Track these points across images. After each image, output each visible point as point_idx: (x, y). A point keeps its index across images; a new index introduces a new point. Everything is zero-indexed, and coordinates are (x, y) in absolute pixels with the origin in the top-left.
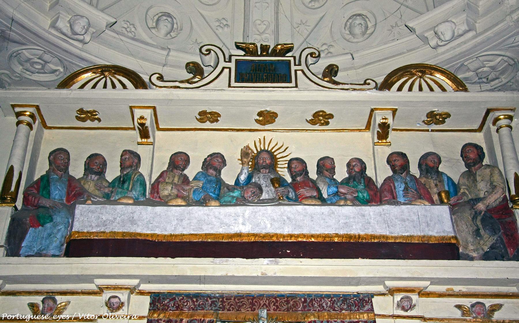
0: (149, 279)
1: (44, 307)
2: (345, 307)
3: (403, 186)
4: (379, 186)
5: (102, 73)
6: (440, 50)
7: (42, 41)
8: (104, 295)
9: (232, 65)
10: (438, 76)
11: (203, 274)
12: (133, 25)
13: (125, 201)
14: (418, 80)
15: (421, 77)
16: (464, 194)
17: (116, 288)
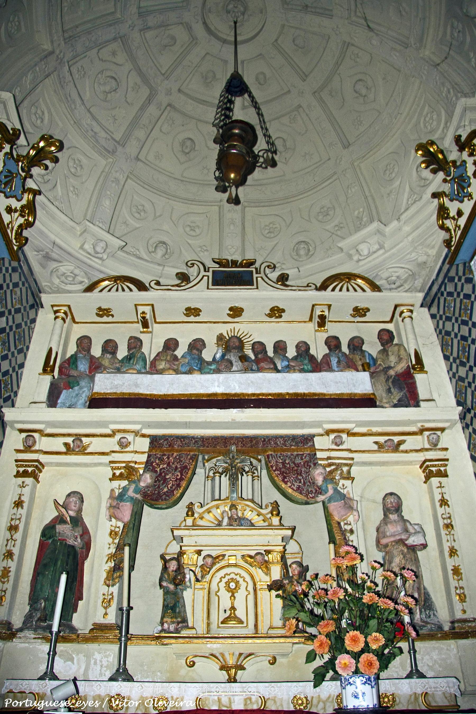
0: (149, 425)
1: (74, 445)
2: (294, 444)
3: (336, 360)
4: (319, 361)
5: (115, 281)
6: (361, 263)
7: (73, 259)
8: (116, 437)
9: (210, 274)
10: (359, 281)
11: (188, 420)
12: (138, 250)
13: (131, 371)
14: (346, 284)
15: (348, 282)
16: (380, 365)
17: (125, 431)
